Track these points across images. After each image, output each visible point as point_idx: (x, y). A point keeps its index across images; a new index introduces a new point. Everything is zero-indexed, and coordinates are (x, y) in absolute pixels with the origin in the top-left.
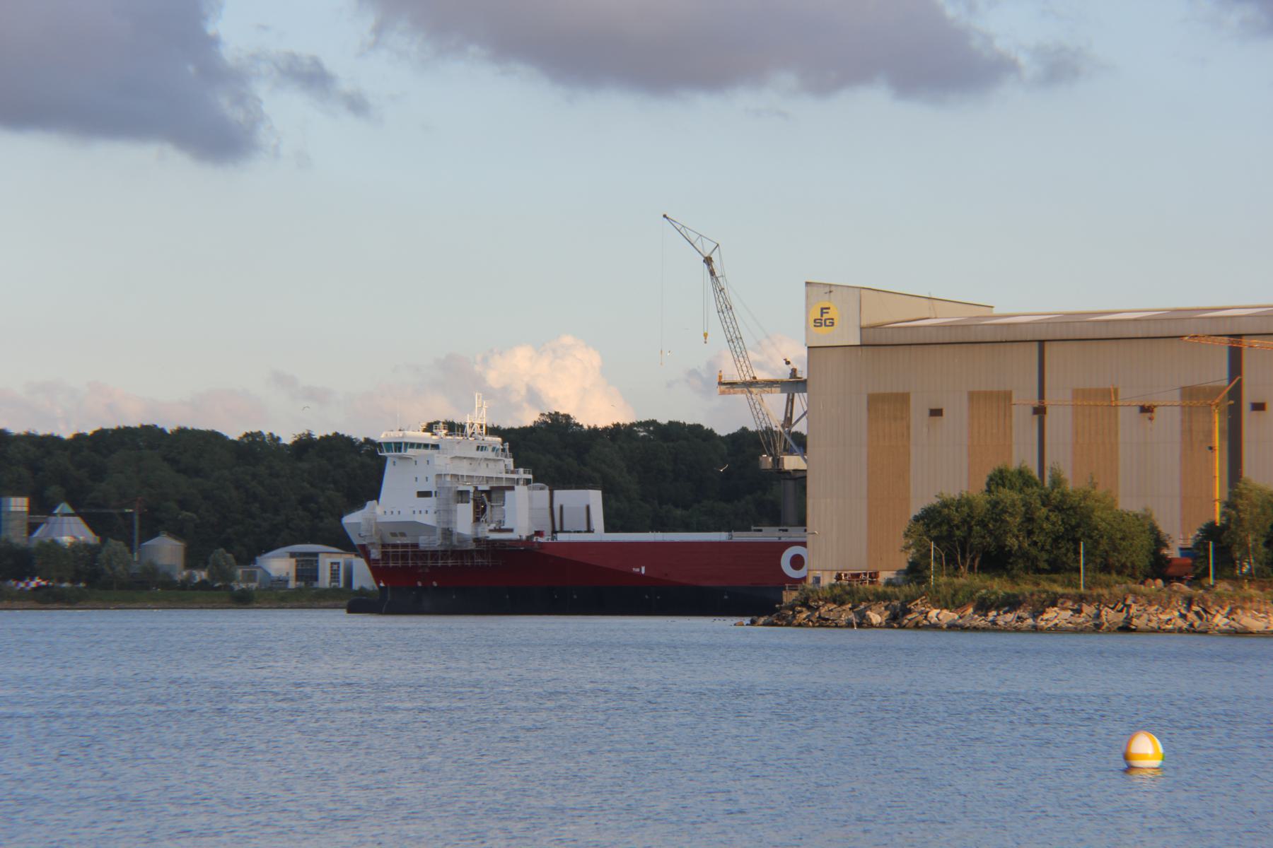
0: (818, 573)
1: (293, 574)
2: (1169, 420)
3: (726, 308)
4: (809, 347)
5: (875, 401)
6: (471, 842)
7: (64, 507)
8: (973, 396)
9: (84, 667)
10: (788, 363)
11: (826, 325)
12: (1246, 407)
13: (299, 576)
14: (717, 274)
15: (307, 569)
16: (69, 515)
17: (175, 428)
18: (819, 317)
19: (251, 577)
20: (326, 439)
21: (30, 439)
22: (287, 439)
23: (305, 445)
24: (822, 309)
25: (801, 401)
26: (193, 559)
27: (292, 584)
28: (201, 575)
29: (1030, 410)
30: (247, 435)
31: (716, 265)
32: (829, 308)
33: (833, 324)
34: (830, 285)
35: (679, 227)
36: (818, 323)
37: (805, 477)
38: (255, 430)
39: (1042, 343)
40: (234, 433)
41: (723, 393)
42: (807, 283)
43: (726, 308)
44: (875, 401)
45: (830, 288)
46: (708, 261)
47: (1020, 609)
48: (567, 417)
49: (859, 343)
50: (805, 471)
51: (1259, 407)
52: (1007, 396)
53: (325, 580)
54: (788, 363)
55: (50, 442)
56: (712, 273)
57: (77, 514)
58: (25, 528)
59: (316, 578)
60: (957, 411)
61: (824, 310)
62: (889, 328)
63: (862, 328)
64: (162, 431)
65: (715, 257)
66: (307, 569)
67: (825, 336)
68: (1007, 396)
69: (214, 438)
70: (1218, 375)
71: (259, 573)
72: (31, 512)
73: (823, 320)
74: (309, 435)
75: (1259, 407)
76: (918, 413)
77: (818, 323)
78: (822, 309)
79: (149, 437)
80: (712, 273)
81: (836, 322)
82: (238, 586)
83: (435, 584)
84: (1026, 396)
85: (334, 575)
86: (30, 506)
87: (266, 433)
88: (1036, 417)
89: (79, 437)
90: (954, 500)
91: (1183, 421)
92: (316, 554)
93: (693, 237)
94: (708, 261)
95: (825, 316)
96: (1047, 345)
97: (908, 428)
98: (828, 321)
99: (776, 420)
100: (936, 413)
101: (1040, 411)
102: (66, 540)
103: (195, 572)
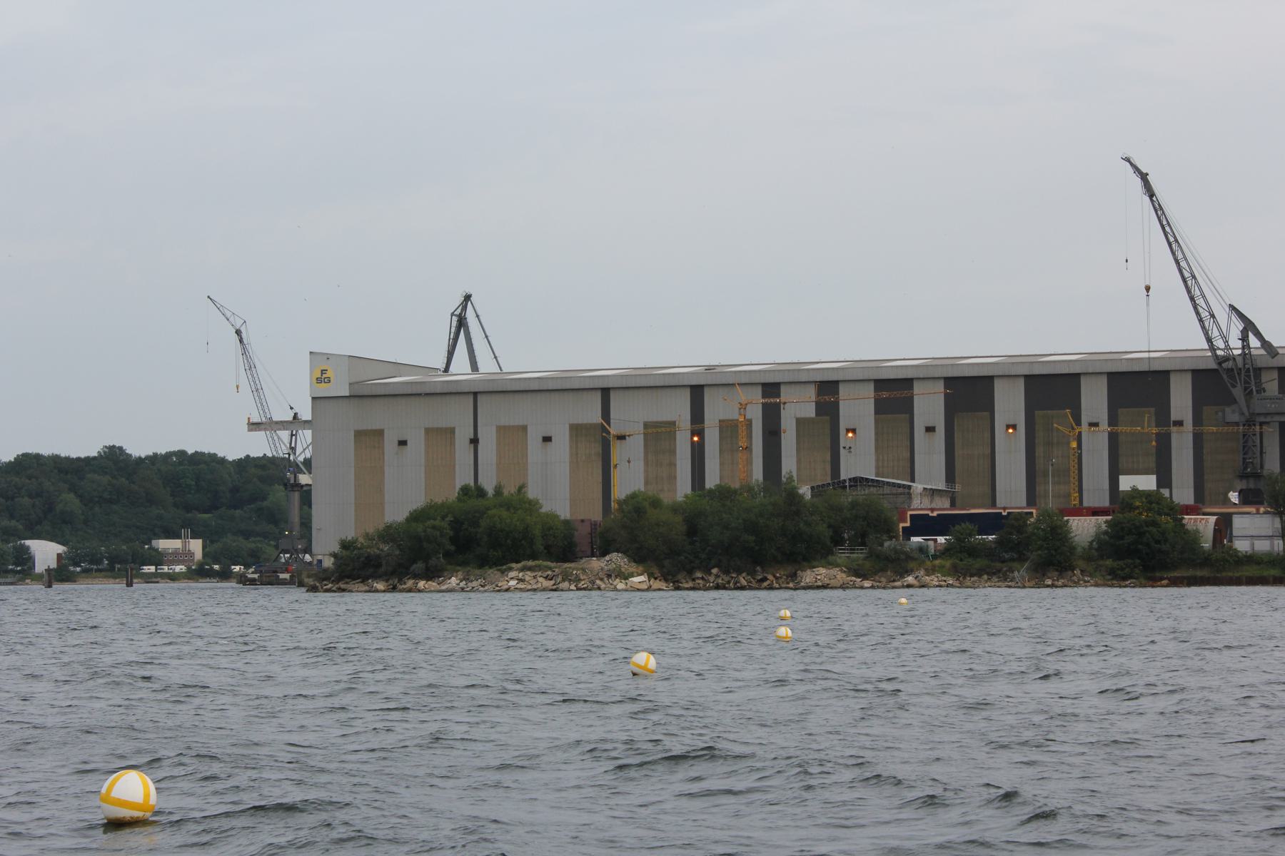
0: (320, 557)
3: (251, 367)
4: (313, 398)
5: (359, 434)
6: (1197, 626)
8: (428, 431)
9: (481, 622)
10: (292, 408)
11: (325, 382)
14: (245, 342)
17: (51, 454)
18: (320, 376)
24: (322, 371)
25: (306, 436)
29: (468, 441)
31: (244, 335)
32: (327, 370)
33: (329, 381)
34: (327, 354)
35: (219, 306)
36: (319, 380)
37: (310, 490)
39: (475, 394)
41: (249, 430)
42: (311, 352)
43: (251, 367)
44: (359, 434)
45: (328, 357)
46: (238, 332)
48: (120, 448)
49: (348, 394)
50: (310, 485)
51: (622, 438)
52: (452, 431)
54: (292, 408)
56: (241, 341)
61: (323, 372)
62: (368, 384)
63: (350, 384)
65: (243, 330)
67: (324, 390)
68: (452, 431)
70: (595, 417)
73: (322, 379)
74: (225, 457)
75: (622, 438)
77: (319, 380)
78: (322, 371)
80: (241, 341)
81: (332, 379)
84: (463, 434)
88: (472, 445)
90: (512, 495)
91: (571, 447)
93: (228, 314)
95: (324, 376)
96: (479, 397)
97: (383, 454)
98: (326, 380)
99: (282, 451)
101: (475, 441)
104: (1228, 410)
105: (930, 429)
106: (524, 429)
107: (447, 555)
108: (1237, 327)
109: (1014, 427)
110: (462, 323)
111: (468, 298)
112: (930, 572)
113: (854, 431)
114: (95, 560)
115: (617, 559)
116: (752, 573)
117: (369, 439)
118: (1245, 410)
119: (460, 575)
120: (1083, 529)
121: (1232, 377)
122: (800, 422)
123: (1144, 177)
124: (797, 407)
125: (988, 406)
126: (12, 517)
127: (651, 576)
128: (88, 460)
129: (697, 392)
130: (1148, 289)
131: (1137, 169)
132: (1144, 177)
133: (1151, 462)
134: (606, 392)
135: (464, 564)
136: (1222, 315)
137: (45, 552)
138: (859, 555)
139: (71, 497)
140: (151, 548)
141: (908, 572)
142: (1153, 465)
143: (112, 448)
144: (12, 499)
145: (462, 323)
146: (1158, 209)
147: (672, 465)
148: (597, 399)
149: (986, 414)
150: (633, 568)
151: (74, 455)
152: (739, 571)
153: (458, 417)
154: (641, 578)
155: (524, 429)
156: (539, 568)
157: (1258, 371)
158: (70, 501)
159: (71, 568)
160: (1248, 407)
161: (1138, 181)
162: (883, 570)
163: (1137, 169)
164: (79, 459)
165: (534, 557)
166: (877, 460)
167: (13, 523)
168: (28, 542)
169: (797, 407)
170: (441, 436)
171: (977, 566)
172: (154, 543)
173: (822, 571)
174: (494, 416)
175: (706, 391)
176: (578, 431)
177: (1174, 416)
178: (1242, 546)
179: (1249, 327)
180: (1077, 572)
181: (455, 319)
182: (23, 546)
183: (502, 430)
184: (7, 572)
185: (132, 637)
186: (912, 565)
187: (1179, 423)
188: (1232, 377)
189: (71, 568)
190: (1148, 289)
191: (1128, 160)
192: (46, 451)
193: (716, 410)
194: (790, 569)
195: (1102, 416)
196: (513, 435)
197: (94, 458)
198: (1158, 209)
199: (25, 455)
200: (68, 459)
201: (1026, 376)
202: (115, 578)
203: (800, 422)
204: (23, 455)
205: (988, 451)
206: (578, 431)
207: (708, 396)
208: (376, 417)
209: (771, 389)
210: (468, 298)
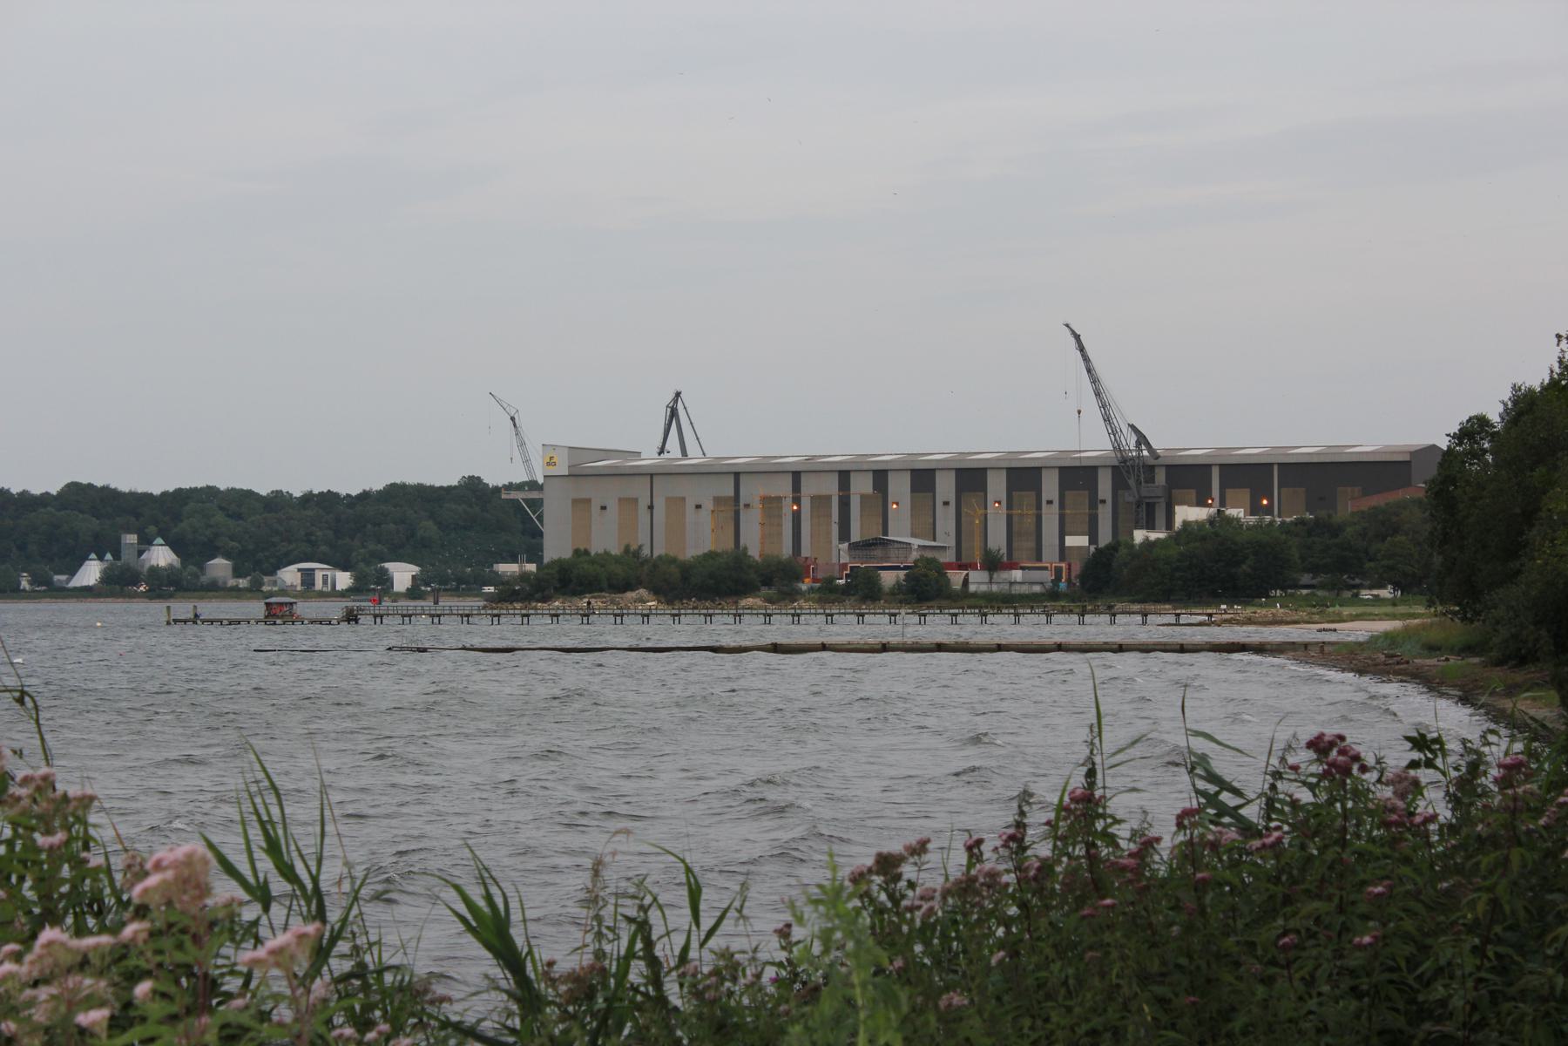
1: (299, 582)
2: (705, 515)
5: (575, 502)
7: (159, 540)
8: (620, 500)
12: (1044, 503)
13: (303, 584)
15: (308, 577)
16: (162, 545)
19: (275, 583)
20: (321, 494)
21: (132, 495)
22: (297, 494)
23: (308, 498)
26: (237, 573)
27: (299, 588)
28: (243, 583)
30: (273, 492)
36: (548, 464)
38: (279, 489)
39: (652, 475)
40: (263, 490)
44: (575, 502)
45: (554, 447)
46: (513, 419)
47: (1431, 604)
48: (479, 478)
51: (747, 506)
52: (636, 500)
53: (319, 585)
55: (147, 497)
56: (515, 425)
57: (166, 544)
58: (136, 553)
59: (314, 585)
60: (613, 507)
61: (551, 458)
64: (218, 489)
66: (308, 577)
69: (249, 494)
70: (731, 493)
71: (279, 582)
72: (138, 543)
73: (551, 463)
75: (747, 506)
76: (595, 509)
79: (210, 492)
80: (515, 425)
82: (265, 588)
83: (1265, 502)
84: (644, 502)
85: (325, 582)
86: (138, 539)
87: (284, 491)
89: (165, 494)
92: (313, 570)
93: (505, 406)
94: (513, 419)
96: (654, 477)
100: (604, 508)
101: (651, 507)
102: (162, 563)
103: (241, 581)
104: (1126, 494)
105: (946, 503)
106: (683, 499)
107: (555, 589)
108: (1132, 440)
109: (999, 503)
110: (673, 414)
111: (678, 394)
112: (806, 601)
113: (897, 504)
114: (443, 581)
115: (643, 592)
116: (713, 601)
117: (582, 504)
118: (1136, 494)
119: (561, 600)
120: (888, 579)
121: (1128, 472)
122: (863, 497)
123: (1077, 337)
124: (862, 486)
125: (982, 488)
126: (379, 542)
127: (659, 601)
128: (449, 489)
129: (796, 476)
130: (1079, 412)
131: (1073, 333)
132: (1077, 337)
133: (1086, 528)
134: (737, 475)
135: (564, 594)
136: (1125, 429)
137: (402, 575)
138: (772, 592)
139: (430, 524)
140: (492, 571)
141: (796, 601)
142: (1087, 529)
143: (471, 478)
144: (379, 525)
145: (673, 414)
146: (1086, 359)
147: (780, 525)
148: (731, 479)
149: (982, 494)
150: (651, 596)
151: (437, 484)
152: (706, 600)
153: (640, 490)
154: (653, 603)
155: (683, 499)
156: (599, 597)
157: (1152, 468)
158: (428, 528)
159: (423, 588)
160: (1138, 492)
161: (1073, 340)
162: (784, 599)
163: (1073, 333)
164: (441, 488)
165: (601, 590)
166: (912, 524)
167: (380, 547)
168: (387, 565)
169: (862, 486)
170: (629, 503)
171: (832, 598)
172: (495, 566)
173: (751, 600)
174: (663, 489)
175: (802, 474)
176: (718, 501)
177: (1101, 496)
178: (972, 588)
179: (1142, 440)
180: (882, 602)
181: (669, 410)
182: (382, 568)
183: (669, 500)
184: (369, 590)
185: (816, 699)
186: (798, 597)
187: (1103, 502)
188: (1128, 472)
189: (423, 588)
190: (1079, 412)
191: (1067, 326)
192: (412, 480)
193: (809, 488)
194: (735, 599)
195: (1055, 497)
196: (677, 503)
197: (455, 487)
198: (1086, 359)
199: (393, 485)
200: (432, 488)
201: (1007, 469)
202: (459, 596)
203: (863, 497)
204: (392, 485)
205: (931, 520)
206: (718, 501)
207: (804, 478)
208: (586, 490)
209: (844, 476)
210: (678, 394)
